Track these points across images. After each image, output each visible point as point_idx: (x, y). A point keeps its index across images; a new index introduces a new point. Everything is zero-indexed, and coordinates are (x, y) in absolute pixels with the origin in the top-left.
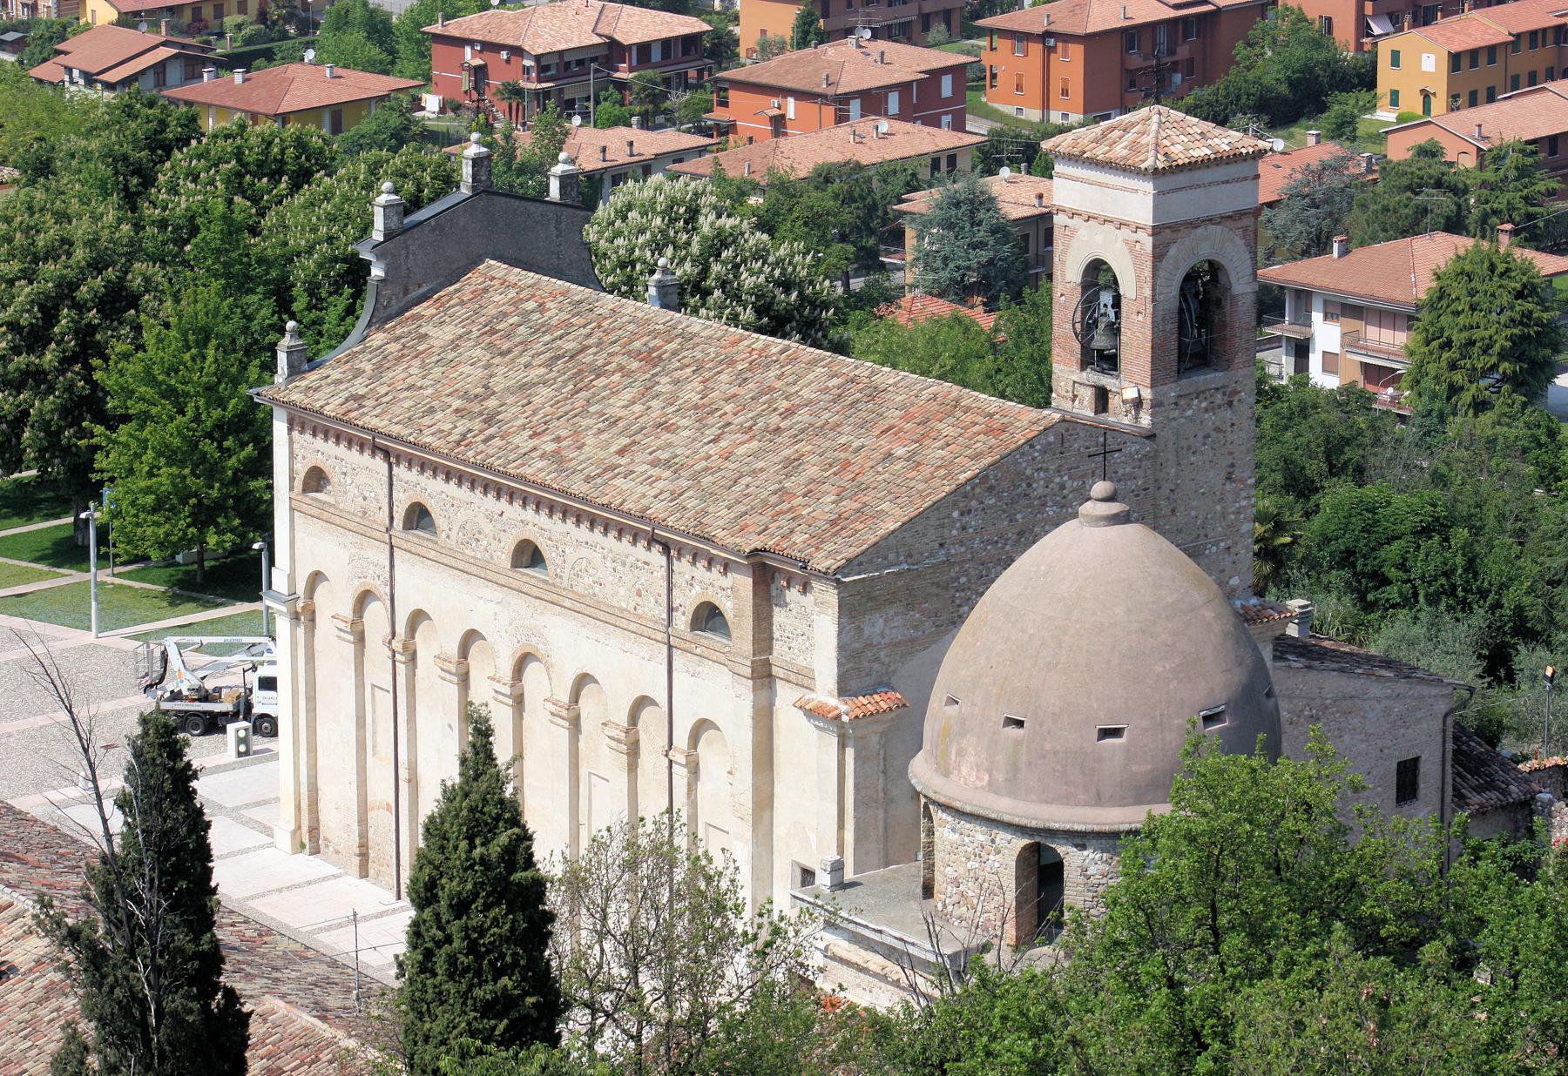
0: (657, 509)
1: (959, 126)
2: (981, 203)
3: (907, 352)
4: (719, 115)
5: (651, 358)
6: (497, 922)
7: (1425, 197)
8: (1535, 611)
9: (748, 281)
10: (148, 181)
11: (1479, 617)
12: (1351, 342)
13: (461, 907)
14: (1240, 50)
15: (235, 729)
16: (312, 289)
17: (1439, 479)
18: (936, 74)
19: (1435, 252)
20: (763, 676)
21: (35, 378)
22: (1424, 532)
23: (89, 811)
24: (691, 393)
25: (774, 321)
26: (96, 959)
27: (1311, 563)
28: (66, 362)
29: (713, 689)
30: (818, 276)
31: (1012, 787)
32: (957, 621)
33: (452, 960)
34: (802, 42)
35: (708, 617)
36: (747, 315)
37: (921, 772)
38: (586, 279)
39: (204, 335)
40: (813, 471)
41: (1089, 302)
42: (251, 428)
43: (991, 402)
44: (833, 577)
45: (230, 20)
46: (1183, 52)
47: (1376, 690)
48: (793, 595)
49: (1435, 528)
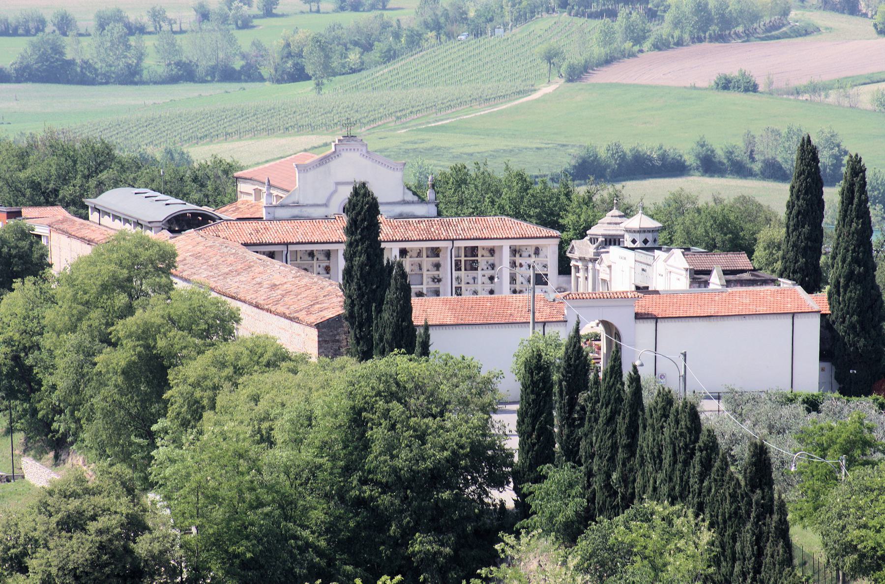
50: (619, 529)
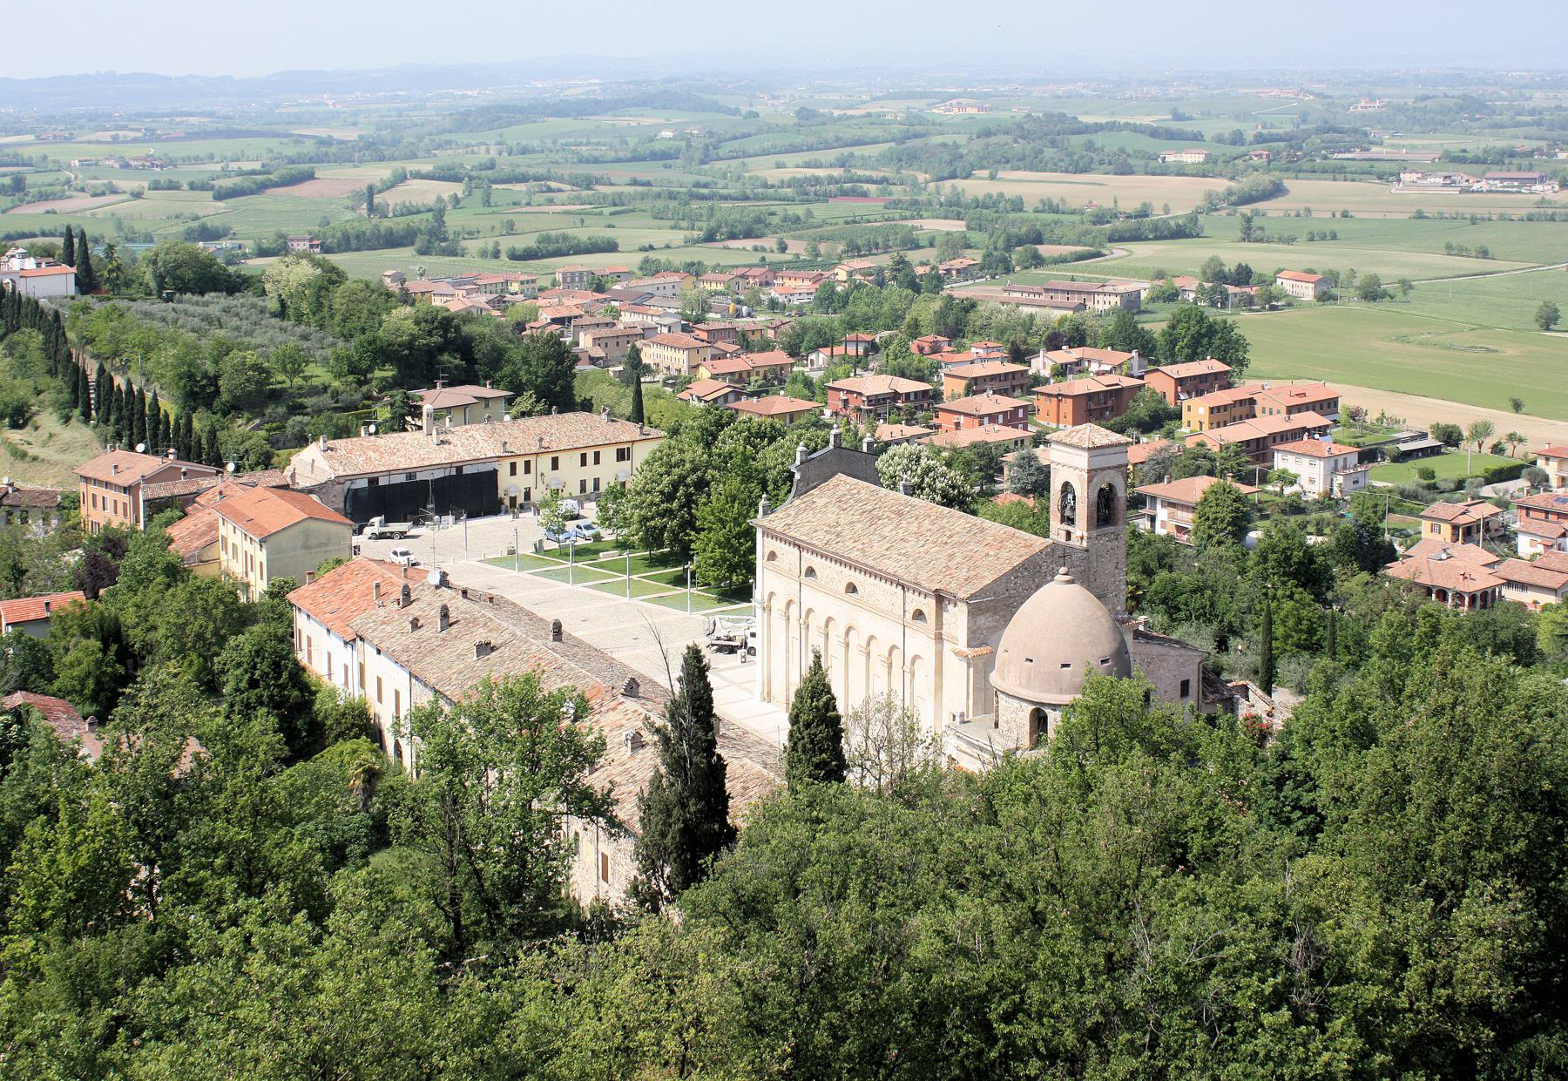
0: (900, 572)
1: (1025, 429)
2: (1031, 459)
3: (1000, 515)
4: (935, 421)
5: (899, 514)
6: (822, 732)
7: (1200, 462)
8: (1236, 624)
9: (939, 485)
10: (715, 438)
11: (1215, 626)
12: (1171, 517)
13: (808, 726)
14: (1131, 403)
15: (741, 652)
16: (775, 482)
17: (1201, 571)
18: (1017, 408)
19: (1201, 485)
20: (939, 638)
21: (669, 513)
22: (1194, 591)
23: (669, 679)
24: (913, 528)
25: (948, 501)
26: (666, 740)
27: (1151, 602)
28: (681, 507)
29: (920, 642)
30: (969, 485)
31: (1028, 685)
32: (1007, 622)
33: (804, 746)
34: (967, 395)
35: (919, 615)
36: (938, 498)
37: (994, 678)
38: (877, 482)
39: (734, 498)
40: (959, 559)
41: (1064, 498)
42: (750, 534)
43: (1027, 535)
44: (966, 601)
45: (753, 378)
46: (1110, 403)
47: (1173, 652)
48: (950, 607)
49: (1199, 590)
50: (15, 337)
